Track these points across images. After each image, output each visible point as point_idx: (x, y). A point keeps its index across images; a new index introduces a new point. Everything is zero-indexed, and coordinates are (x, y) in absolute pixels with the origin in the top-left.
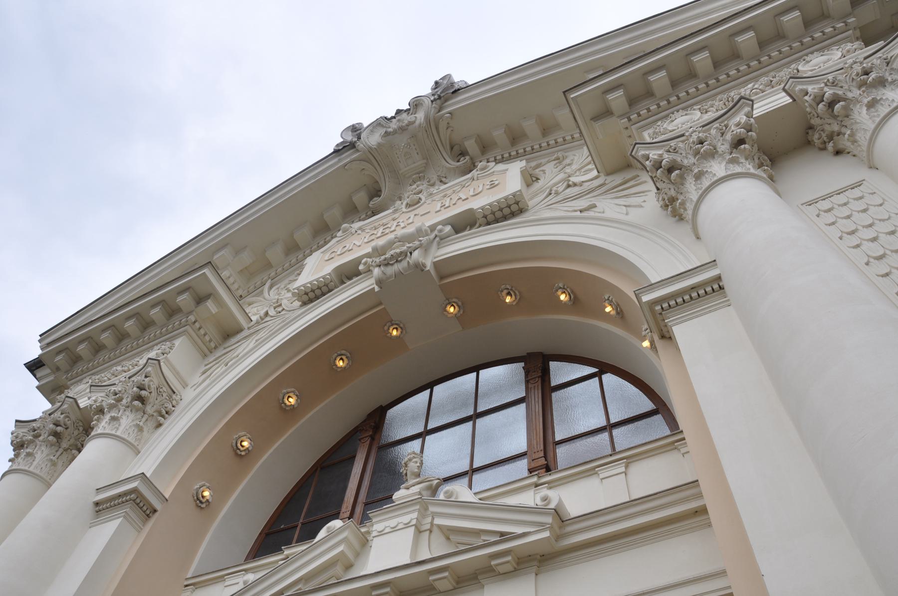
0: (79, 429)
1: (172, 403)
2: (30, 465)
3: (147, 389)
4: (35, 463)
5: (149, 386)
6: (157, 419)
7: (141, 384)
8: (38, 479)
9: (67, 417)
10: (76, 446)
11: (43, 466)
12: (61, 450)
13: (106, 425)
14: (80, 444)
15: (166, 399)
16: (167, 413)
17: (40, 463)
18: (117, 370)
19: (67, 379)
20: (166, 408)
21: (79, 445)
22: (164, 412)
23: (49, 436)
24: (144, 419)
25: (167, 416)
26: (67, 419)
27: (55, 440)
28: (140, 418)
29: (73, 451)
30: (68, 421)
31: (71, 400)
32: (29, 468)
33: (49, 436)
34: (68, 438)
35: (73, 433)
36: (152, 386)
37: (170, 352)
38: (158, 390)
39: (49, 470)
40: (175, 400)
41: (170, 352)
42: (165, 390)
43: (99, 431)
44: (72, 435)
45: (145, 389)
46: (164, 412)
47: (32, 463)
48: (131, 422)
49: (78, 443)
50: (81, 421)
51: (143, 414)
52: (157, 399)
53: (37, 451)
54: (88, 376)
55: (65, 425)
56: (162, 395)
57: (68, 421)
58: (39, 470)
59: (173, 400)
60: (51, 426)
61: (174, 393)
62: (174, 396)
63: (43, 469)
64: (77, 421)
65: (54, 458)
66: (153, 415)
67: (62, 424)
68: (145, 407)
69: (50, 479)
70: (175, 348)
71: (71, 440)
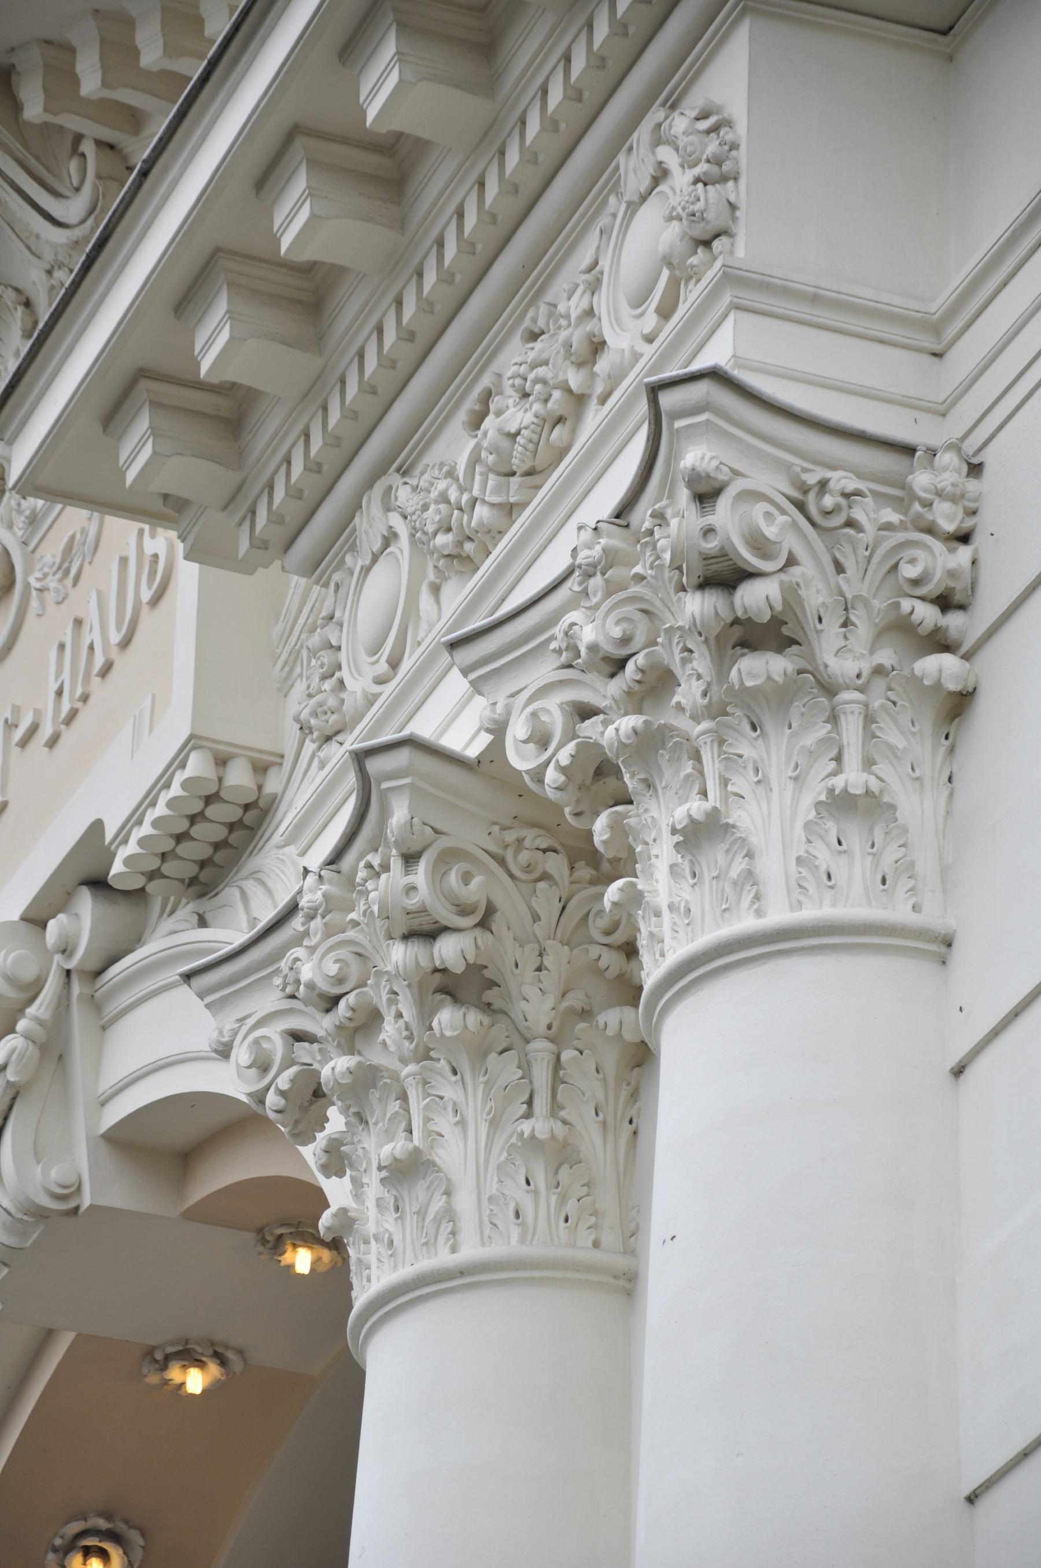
0: (545, 877)
1: (930, 530)
2: (446, 1228)
3: (753, 561)
4: (465, 1202)
5: (760, 545)
6: (915, 681)
7: (706, 558)
8: (532, 1281)
9: (448, 857)
10: (596, 970)
11: (517, 1192)
12: (541, 1049)
13: (686, 893)
14: (606, 954)
15: (888, 527)
16: (945, 602)
17: (492, 1187)
18: (513, 436)
19: (265, 545)
20: (916, 582)
21: (612, 961)
22: (926, 614)
23: (426, 1015)
24: (851, 730)
25: (954, 621)
26: (453, 879)
27: (474, 1018)
28: (822, 741)
29: (601, 1019)
30: (466, 878)
31: (402, 757)
32: (454, 1250)
33: (426, 1015)
34: (528, 958)
35: (536, 918)
36: (770, 531)
37: (733, 207)
38: (813, 509)
39: (563, 1200)
40: (939, 494)
41: (733, 207)
42: (852, 484)
43: (677, 951)
44: (539, 930)
45: (747, 575)
46: (926, 614)
47: (449, 1214)
48: (796, 800)
49: (594, 951)
50: (532, 825)
51: (824, 700)
52: (840, 568)
53: (427, 1120)
54: (369, 483)
55: (464, 911)
56: (850, 523)
57: (466, 878)
58: (515, 1233)
59: (928, 505)
60: (399, 954)
61: (908, 450)
62: (921, 480)
63: (528, 1211)
64: (510, 837)
65: (540, 1126)
66: (879, 671)
67: (447, 916)
68: (811, 657)
69: (596, 1244)
70: (741, 129)
71: (547, 961)
